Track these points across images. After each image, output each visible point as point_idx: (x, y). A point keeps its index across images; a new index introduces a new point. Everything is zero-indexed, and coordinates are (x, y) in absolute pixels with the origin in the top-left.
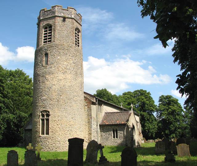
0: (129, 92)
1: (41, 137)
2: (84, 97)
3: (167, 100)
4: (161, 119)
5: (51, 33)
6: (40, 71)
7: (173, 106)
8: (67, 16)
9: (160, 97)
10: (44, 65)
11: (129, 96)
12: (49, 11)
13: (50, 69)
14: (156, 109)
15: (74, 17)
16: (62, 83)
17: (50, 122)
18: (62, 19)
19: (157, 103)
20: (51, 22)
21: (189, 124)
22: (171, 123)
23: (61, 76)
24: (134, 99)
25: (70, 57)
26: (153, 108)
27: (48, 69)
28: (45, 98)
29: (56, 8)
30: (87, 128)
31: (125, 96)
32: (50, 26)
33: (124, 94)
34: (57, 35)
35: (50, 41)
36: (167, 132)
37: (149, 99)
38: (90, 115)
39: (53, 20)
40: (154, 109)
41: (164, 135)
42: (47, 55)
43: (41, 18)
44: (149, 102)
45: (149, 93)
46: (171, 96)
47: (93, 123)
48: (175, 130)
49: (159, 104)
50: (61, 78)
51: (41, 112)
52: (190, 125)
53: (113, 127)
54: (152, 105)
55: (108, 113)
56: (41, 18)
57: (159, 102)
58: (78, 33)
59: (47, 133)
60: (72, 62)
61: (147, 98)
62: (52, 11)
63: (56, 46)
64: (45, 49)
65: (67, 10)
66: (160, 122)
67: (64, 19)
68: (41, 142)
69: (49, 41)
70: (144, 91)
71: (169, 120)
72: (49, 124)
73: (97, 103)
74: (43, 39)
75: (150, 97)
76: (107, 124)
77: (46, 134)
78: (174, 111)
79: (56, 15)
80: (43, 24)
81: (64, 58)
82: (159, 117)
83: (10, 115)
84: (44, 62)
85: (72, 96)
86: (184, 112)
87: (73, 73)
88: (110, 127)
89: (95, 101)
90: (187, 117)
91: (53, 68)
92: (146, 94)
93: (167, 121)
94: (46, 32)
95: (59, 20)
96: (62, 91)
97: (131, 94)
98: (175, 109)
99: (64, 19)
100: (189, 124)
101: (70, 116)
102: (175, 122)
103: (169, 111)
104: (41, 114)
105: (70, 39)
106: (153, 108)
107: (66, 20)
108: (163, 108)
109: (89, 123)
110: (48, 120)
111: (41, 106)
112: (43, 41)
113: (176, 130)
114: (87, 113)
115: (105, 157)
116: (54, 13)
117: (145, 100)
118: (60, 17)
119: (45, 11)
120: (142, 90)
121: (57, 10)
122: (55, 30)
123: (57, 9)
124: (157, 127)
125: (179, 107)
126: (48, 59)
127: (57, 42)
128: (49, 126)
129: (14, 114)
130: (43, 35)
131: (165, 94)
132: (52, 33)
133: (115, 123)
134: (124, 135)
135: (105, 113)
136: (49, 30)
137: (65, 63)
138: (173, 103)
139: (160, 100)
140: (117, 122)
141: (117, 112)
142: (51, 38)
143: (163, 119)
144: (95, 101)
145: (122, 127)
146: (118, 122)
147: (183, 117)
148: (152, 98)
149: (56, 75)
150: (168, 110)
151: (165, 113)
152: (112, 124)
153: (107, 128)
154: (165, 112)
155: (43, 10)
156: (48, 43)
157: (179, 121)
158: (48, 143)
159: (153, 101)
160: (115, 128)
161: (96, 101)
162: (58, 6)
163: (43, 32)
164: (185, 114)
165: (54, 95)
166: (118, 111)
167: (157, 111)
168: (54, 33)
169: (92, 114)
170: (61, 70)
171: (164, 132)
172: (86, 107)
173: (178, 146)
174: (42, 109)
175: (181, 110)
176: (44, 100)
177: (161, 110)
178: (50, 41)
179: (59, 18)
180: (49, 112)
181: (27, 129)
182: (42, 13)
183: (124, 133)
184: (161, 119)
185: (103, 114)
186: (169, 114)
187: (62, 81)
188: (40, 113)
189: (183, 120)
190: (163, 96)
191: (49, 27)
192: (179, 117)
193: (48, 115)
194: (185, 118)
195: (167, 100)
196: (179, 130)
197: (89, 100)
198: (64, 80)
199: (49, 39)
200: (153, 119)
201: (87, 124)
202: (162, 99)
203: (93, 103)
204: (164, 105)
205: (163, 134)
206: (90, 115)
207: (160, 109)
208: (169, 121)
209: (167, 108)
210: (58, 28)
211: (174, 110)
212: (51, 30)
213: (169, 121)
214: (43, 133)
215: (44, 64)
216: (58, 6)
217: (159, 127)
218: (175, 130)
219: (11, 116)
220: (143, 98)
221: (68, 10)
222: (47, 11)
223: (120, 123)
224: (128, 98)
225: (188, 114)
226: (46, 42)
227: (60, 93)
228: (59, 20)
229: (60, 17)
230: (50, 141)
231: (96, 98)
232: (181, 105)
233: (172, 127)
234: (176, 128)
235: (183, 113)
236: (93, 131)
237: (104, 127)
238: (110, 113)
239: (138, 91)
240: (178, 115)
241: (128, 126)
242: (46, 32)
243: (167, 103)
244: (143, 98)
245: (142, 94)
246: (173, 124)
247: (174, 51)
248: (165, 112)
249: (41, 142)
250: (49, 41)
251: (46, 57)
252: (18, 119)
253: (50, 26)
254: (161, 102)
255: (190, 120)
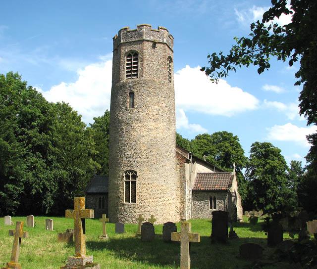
0: (205, 135)
1: (125, 205)
2: (176, 152)
3: (263, 149)
4: (252, 180)
5: (137, 63)
6: (123, 116)
7: (273, 160)
8: (157, 40)
9: (253, 145)
10: (128, 108)
11: (205, 141)
12: (133, 31)
13: (137, 115)
14: (247, 163)
15: (167, 41)
16: (153, 134)
17: (138, 186)
18: (151, 44)
19: (247, 154)
20: (136, 48)
21: (296, 189)
22: (268, 187)
23: (152, 125)
24: (213, 147)
25: (163, 99)
26: (243, 162)
27: (134, 115)
28: (131, 153)
29: (144, 29)
30: (179, 194)
31: (200, 141)
32: (136, 54)
33: (198, 138)
34: (146, 69)
35: (136, 75)
36: (261, 200)
37: (237, 147)
38: (182, 178)
39: (140, 45)
40: (243, 164)
41: (256, 205)
42: (132, 94)
43: (122, 41)
44: (237, 153)
45: (236, 138)
46: (270, 144)
47: (187, 188)
48: (274, 198)
49: (250, 156)
50: (152, 127)
51: (126, 172)
52: (297, 192)
53: (210, 194)
54: (241, 157)
55: (202, 174)
56: (122, 41)
57: (251, 152)
58: (170, 63)
59: (134, 201)
60: (164, 105)
61: (233, 145)
62: (138, 32)
63: (145, 83)
64: (129, 86)
65: (157, 31)
66: (251, 184)
67: (154, 44)
68: (125, 211)
69: (134, 75)
70: (228, 134)
71: (266, 181)
72: (135, 189)
73: (191, 160)
74: (125, 69)
75: (238, 144)
76: (202, 189)
77: (132, 202)
78: (274, 168)
79: (144, 38)
80: (125, 50)
81: (155, 99)
82: (250, 176)
83: (64, 172)
84: (128, 104)
85: (164, 152)
86: (288, 170)
87: (166, 120)
88: (206, 194)
89: (188, 158)
90: (292, 178)
91: (141, 113)
92: (232, 140)
93: (263, 184)
94: (130, 62)
95: (148, 46)
96: (152, 145)
97: (209, 138)
98: (276, 164)
99: (154, 44)
100: (296, 189)
101: (162, 179)
102: (274, 185)
103: (265, 168)
104: (124, 174)
105: (162, 73)
106: (241, 162)
107: (157, 45)
108: (257, 161)
109: (182, 188)
110: (134, 183)
111: (125, 164)
112: (126, 74)
113: (276, 198)
114: (179, 174)
115: (312, 221)
116: (141, 35)
117: (230, 148)
118: (148, 41)
119: (127, 32)
120: (225, 133)
121: (145, 31)
122: (142, 61)
123: (146, 30)
124: (247, 192)
125: (281, 162)
126: (135, 101)
127: (146, 77)
128: (137, 192)
129: (67, 170)
130: (126, 66)
131: (261, 141)
132: (139, 65)
133: (213, 189)
134: (224, 205)
135: (198, 174)
136: (134, 60)
137: (157, 107)
138: (272, 155)
139: (253, 150)
140: (216, 187)
141: (209, 174)
142: (137, 71)
143: (255, 180)
144: (188, 158)
145: (223, 194)
146: (217, 188)
147: (287, 177)
148: (240, 146)
149: (146, 123)
150: (264, 166)
151: (261, 171)
152: (209, 189)
153: (203, 194)
154: (260, 169)
155: (125, 29)
156: (132, 77)
157: (280, 184)
158: (134, 214)
159: (242, 151)
160: (213, 195)
161: (190, 158)
162: (146, 26)
163: (125, 61)
164: (290, 174)
165: (143, 150)
166: (211, 171)
167: (247, 166)
168: (142, 65)
169: (186, 176)
170: (152, 116)
171: (258, 200)
172: (178, 166)
173: (52, 241)
174: (126, 169)
175: (285, 166)
176: (130, 156)
177: (253, 166)
178: (136, 75)
179: (147, 43)
180: (136, 172)
181: (89, 192)
182: (124, 33)
183: (225, 203)
184: (252, 180)
185: (195, 176)
186: (266, 172)
187: (154, 131)
188: (124, 174)
189: (287, 183)
190: (257, 143)
191: (134, 56)
192: (281, 178)
193: (135, 177)
194: (289, 180)
195: (263, 149)
196: (279, 198)
197: (182, 156)
198: (155, 131)
199: (134, 71)
200: (241, 179)
201: (179, 189)
202: (256, 147)
203: (187, 161)
204: (259, 158)
205: (255, 204)
206: (182, 178)
207: (252, 163)
208: (265, 184)
209: (263, 163)
210: (147, 57)
211: (274, 166)
212: (137, 59)
213: (265, 184)
214: (128, 200)
215: (128, 107)
216: (146, 26)
217: (250, 192)
218: (274, 198)
219: (64, 173)
220: (227, 145)
221: (159, 32)
222: (131, 31)
223: (221, 189)
224: (204, 144)
225: (294, 173)
226: (130, 76)
227: (150, 147)
228: (148, 46)
229: (148, 41)
230: (137, 211)
231: (190, 154)
232: (284, 159)
233: (270, 193)
234: (274, 196)
235: (287, 172)
236: (187, 198)
237: (197, 194)
238: (204, 174)
239: (219, 133)
240: (279, 174)
241: (230, 193)
242: (130, 62)
243: (262, 154)
244: (227, 145)
245: (225, 139)
246: (271, 189)
247: (302, 101)
248: (260, 169)
249: (125, 211)
250: (134, 75)
251: (130, 97)
252: (72, 177)
253: (136, 54)
254: (253, 153)
255: (296, 183)
